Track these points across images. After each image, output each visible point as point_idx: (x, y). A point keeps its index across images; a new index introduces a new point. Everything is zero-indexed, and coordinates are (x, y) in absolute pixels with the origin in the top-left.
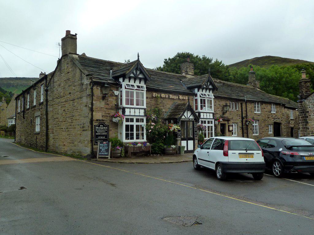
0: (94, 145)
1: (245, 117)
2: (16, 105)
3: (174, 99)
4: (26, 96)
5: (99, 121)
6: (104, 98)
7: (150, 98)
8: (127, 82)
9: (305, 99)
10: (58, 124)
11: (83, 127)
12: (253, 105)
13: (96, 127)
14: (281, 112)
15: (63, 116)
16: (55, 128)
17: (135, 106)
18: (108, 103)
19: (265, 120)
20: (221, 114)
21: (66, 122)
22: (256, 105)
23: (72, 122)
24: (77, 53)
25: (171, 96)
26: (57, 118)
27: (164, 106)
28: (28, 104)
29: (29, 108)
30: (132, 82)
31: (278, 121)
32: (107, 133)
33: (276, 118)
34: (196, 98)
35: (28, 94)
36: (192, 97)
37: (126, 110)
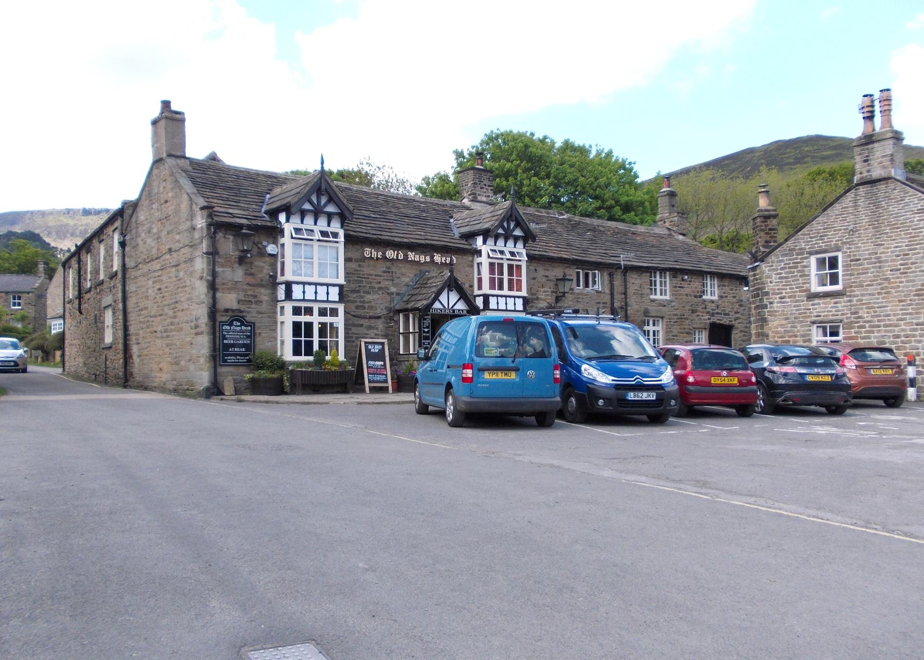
0: (221, 365)
1: (621, 308)
2: (64, 280)
3: (418, 263)
4: (83, 257)
5: (230, 312)
6: (242, 260)
7: (357, 260)
8: (296, 221)
9: (762, 260)
10: (148, 321)
11: (196, 327)
12: (646, 278)
13: (223, 325)
14: (734, 297)
15: (157, 302)
16: (141, 332)
17: (506, 292)
18: (252, 271)
19: (682, 318)
20: (551, 300)
21: (163, 317)
22: (665, 278)
23: (175, 317)
24: (187, 155)
25: (411, 256)
26: (146, 308)
27: (393, 280)
28: (89, 276)
29: (91, 288)
30: (309, 221)
31: (725, 321)
32: (251, 341)
33: (718, 313)
34: (479, 260)
35: (87, 253)
36: (471, 258)
37: (294, 287)
